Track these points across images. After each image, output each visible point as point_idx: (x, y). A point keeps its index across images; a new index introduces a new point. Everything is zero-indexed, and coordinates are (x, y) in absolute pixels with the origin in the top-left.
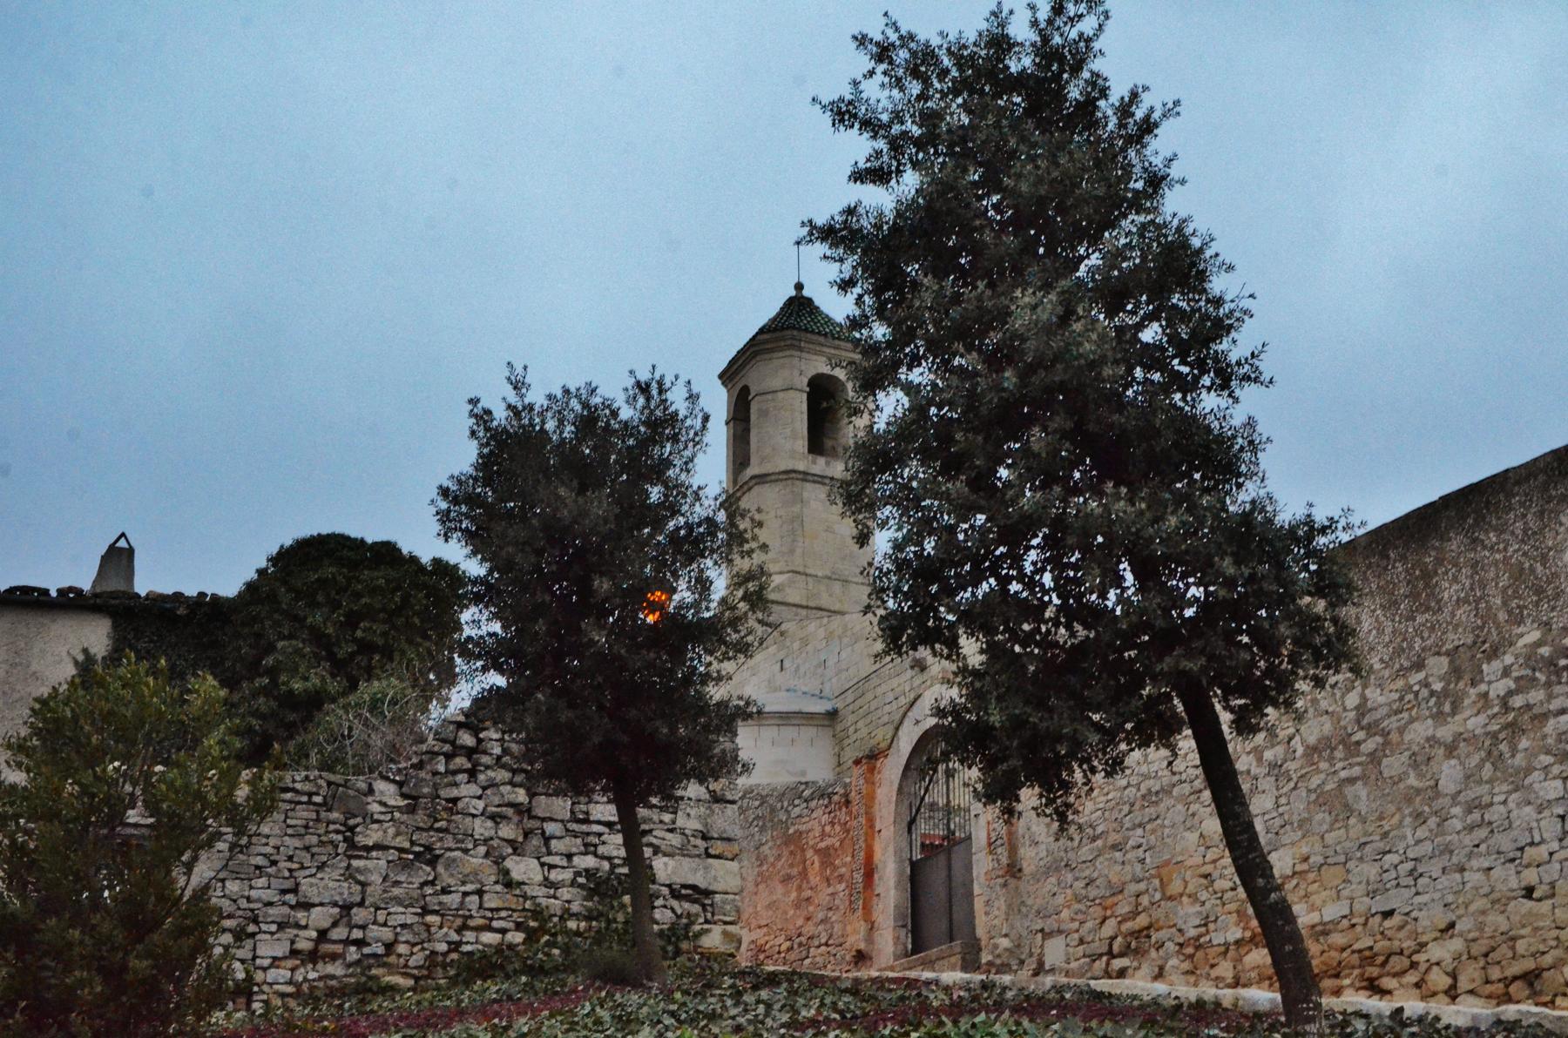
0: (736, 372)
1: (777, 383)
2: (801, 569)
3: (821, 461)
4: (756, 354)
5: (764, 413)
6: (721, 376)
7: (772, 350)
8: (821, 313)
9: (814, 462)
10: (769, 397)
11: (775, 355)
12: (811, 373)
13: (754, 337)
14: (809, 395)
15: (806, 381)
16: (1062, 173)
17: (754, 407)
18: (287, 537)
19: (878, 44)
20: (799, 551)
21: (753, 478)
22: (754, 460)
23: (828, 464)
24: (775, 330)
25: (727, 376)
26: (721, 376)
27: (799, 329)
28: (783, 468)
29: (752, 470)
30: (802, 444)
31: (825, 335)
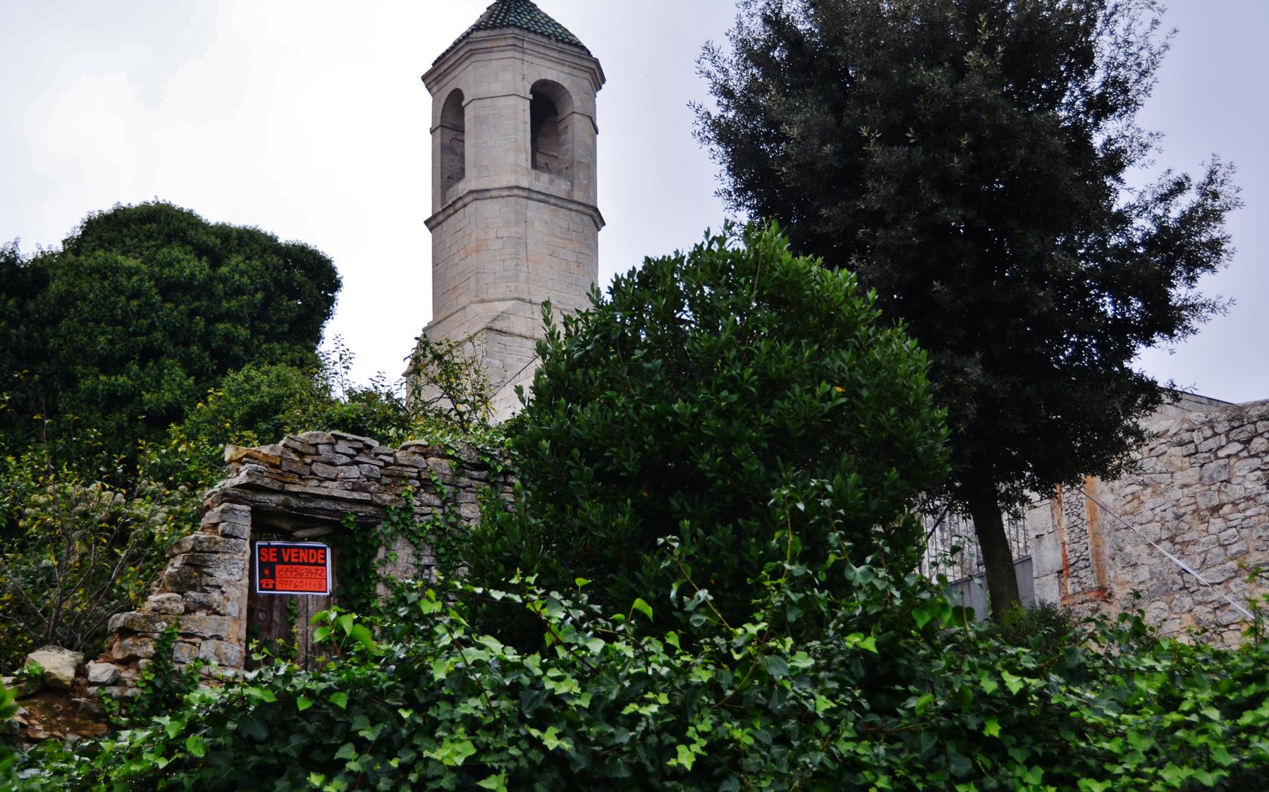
0: (445, 74)
1: (497, 88)
2: (526, 297)
3: (545, 177)
4: (472, 53)
5: (480, 121)
6: (424, 78)
7: (489, 50)
8: (540, 12)
9: (538, 179)
10: (488, 102)
11: (494, 55)
12: (534, 78)
13: (466, 36)
14: (531, 102)
15: (529, 87)
16: (770, 405)
17: (469, 113)
18: (134, 193)
19: (1176, 652)
20: (522, 276)
21: (471, 192)
22: (470, 172)
23: (551, 182)
24: (493, 27)
25: (432, 79)
26: (424, 78)
27: (521, 28)
28: (504, 184)
29: (463, 187)
30: (525, 158)
31: (549, 36)
